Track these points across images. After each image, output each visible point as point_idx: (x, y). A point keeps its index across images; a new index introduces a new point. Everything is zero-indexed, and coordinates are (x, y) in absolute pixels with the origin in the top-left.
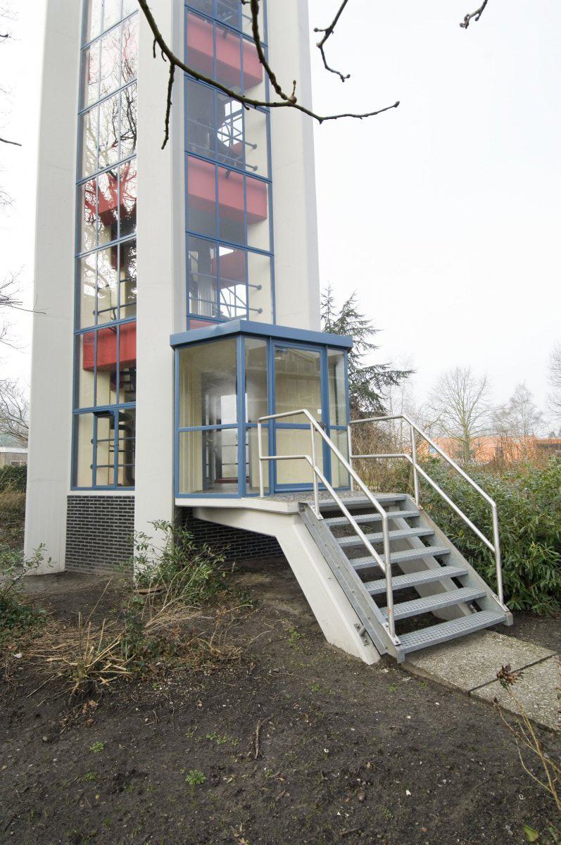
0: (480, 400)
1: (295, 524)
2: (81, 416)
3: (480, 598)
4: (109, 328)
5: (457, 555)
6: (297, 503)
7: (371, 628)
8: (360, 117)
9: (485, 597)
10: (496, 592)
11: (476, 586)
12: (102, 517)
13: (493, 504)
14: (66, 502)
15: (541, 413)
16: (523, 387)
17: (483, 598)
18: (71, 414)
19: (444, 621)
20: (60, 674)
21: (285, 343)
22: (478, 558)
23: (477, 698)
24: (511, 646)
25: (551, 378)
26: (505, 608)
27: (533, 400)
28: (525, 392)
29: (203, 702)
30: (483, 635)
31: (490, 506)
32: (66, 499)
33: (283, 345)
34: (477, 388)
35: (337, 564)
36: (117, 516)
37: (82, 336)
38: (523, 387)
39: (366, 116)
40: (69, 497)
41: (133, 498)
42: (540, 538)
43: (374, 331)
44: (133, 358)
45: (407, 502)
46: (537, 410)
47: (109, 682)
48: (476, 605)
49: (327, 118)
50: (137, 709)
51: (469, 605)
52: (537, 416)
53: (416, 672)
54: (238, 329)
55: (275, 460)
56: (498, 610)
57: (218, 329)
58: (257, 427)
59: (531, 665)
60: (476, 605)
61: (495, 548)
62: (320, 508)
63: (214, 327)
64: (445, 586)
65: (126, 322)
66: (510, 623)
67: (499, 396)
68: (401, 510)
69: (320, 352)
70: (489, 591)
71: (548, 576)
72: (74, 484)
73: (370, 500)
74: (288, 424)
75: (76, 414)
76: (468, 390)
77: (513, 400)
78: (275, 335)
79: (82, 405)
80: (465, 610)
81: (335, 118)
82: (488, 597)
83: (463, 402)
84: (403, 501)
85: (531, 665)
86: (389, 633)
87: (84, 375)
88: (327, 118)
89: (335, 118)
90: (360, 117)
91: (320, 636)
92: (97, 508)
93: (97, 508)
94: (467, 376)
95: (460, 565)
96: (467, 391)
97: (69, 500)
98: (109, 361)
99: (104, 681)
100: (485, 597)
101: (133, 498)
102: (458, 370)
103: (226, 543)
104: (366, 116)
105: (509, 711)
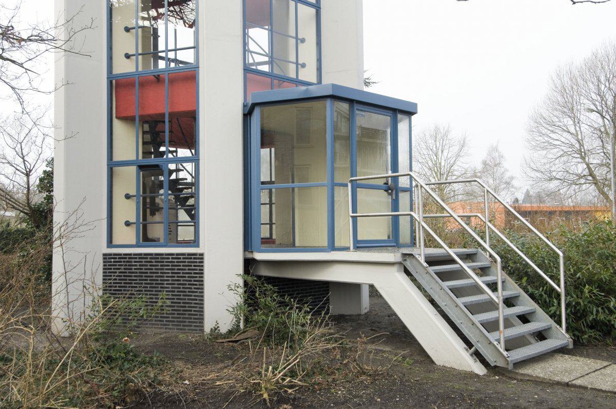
0: (458, 163)
1: (397, 271)
2: (116, 169)
3: (545, 330)
4: (154, 76)
5: (525, 297)
6: (400, 254)
7: (480, 348)
8: (595, 3)
9: (551, 328)
10: (559, 322)
11: (542, 321)
12: (149, 275)
13: (561, 254)
14: (101, 261)
15: (512, 178)
16: (495, 149)
17: (549, 329)
18: (106, 166)
19: (511, 350)
20: (242, 391)
21: (366, 107)
22: (546, 299)
23: (575, 386)
24: (578, 361)
25: (528, 141)
26: (567, 336)
27: (506, 164)
28: (497, 154)
29: (380, 397)
30: (552, 356)
31: (558, 255)
32: (101, 257)
33: (366, 109)
34: (455, 149)
35: (443, 301)
36: (168, 273)
37: (114, 81)
38: (495, 149)
39: (599, 2)
40: (104, 255)
41: (202, 255)
42: (590, 282)
43: (369, 83)
44: (191, 109)
45: (478, 256)
46: (507, 175)
47: (293, 391)
48: (541, 336)
49: (578, 2)
50: (332, 405)
51: (534, 337)
52: (508, 180)
53: (519, 377)
54: (330, 93)
55: (357, 217)
56: (561, 336)
57: (307, 91)
58: (347, 186)
59: (599, 370)
60: (541, 336)
61: (561, 290)
62: (426, 257)
63: (304, 88)
64: (514, 323)
65: (186, 70)
66: (571, 346)
67: (472, 161)
68: (473, 261)
69: (390, 116)
70: (554, 325)
71: (595, 312)
72: (110, 243)
73: (448, 252)
74: (372, 185)
75: (111, 166)
76: (447, 151)
77: (485, 163)
78: (400, 109)
79: (117, 157)
80: (532, 340)
81: (582, 2)
82: (554, 328)
83: (440, 164)
84: (475, 254)
85: (599, 370)
86: (500, 349)
87: (117, 123)
88: (578, 2)
89: (582, 2)
90: (595, 3)
91: (433, 362)
92: (143, 265)
93: (143, 265)
94: (446, 134)
95: (527, 305)
96: (445, 153)
97: (104, 258)
98: (151, 111)
99: (290, 391)
100: (551, 328)
101: (202, 255)
102: (437, 130)
103: (324, 294)
104: (599, 2)
105: (602, 390)
